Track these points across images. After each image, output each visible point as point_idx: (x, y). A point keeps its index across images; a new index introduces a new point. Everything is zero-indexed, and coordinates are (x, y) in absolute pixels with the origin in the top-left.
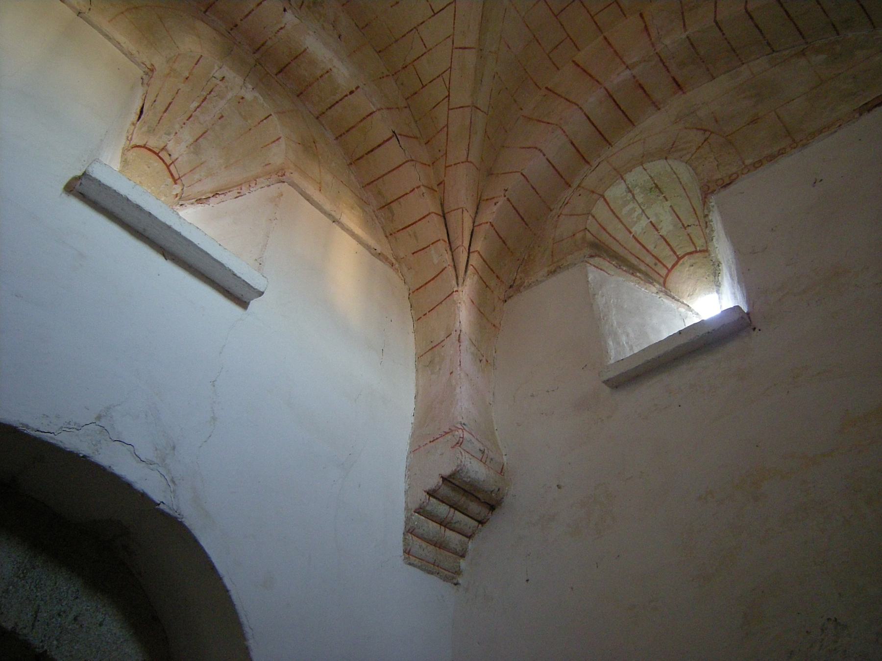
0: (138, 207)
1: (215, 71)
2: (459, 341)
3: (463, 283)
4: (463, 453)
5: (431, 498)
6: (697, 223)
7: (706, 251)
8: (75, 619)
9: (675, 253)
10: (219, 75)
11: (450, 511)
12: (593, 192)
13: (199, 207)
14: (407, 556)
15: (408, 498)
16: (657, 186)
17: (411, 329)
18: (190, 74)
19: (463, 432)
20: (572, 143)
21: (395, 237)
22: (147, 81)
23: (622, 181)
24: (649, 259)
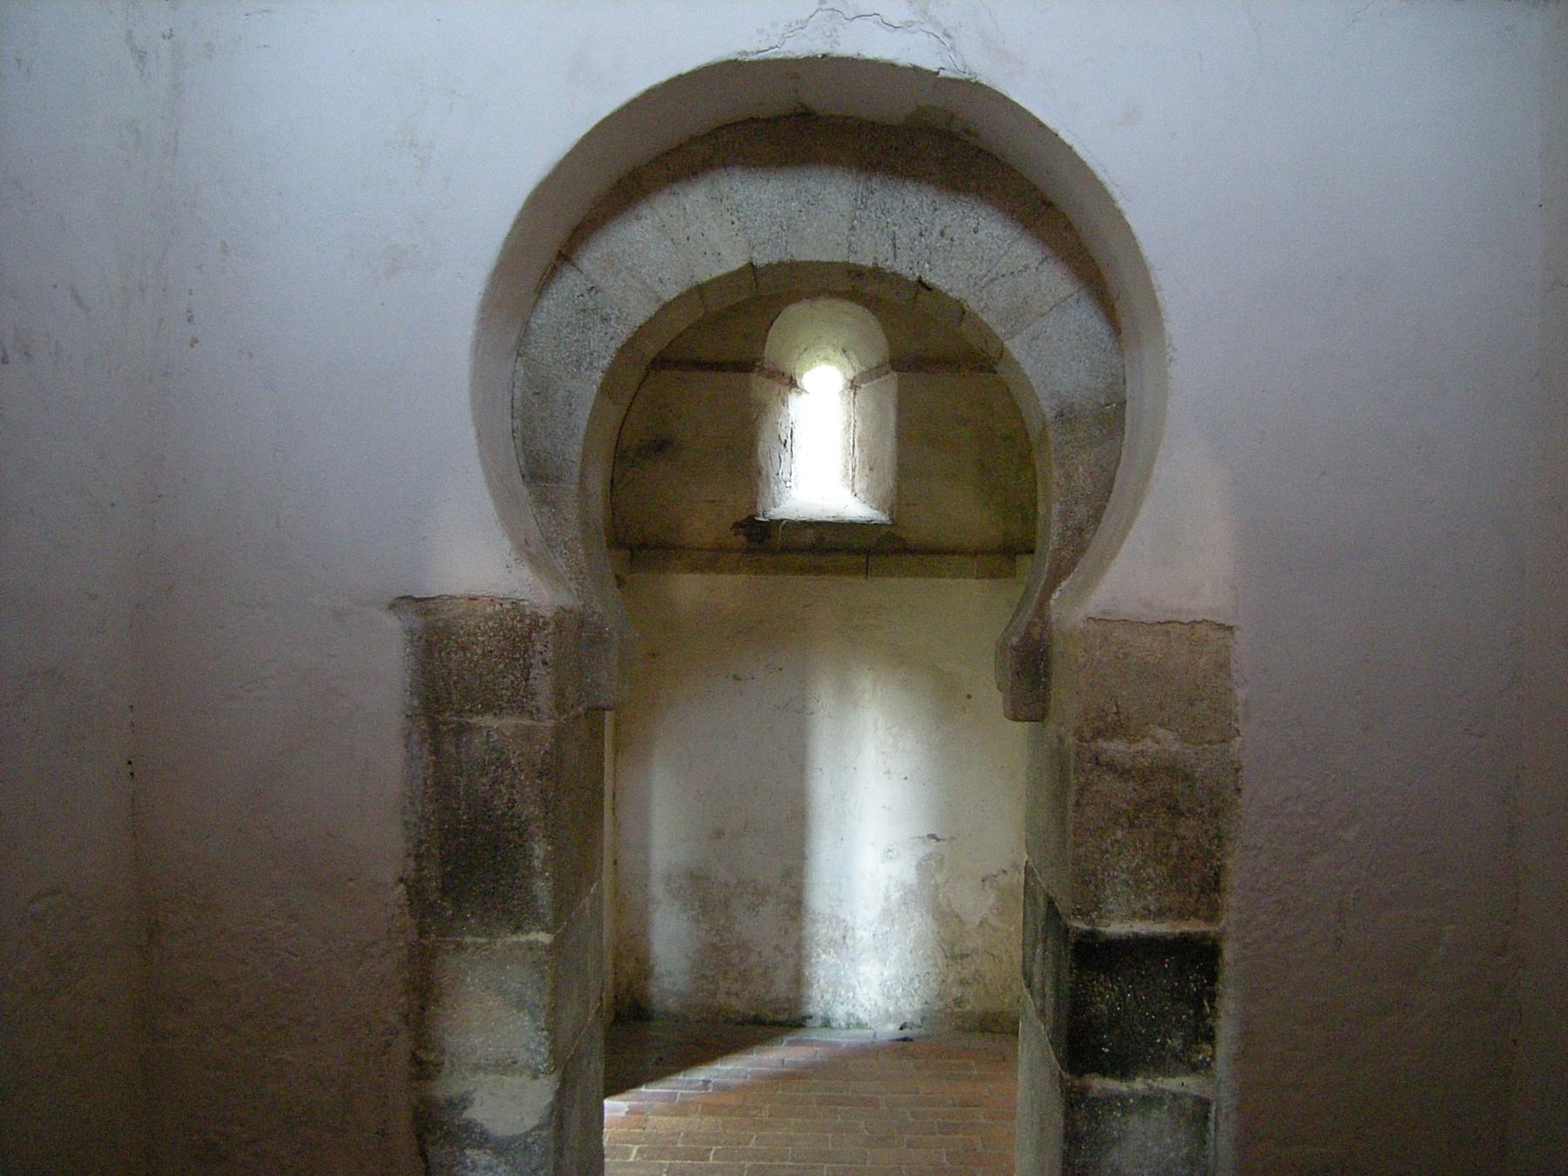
8: (942, 234)
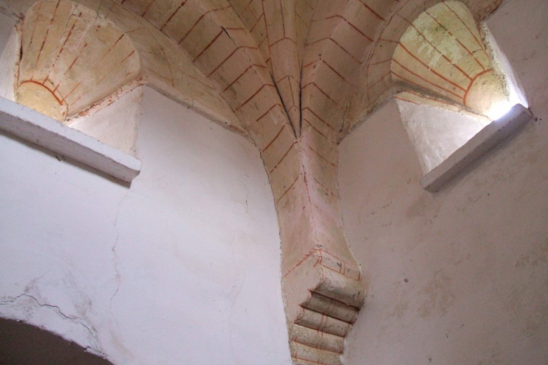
0: (29, 124)
1: (72, 10)
2: (305, 181)
3: (300, 135)
4: (323, 268)
5: (305, 310)
6: (480, 48)
7: (491, 70)
9: (468, 76)
10: (76, 12)
11: (323, 317)
12: (391, 41)
13: (82, 119)
14: (294, 359)
15: (288, 314)
16: (441, 26)
17: (267, 181)
18: (54, 16)
19: (321, 252)
20: (366, 6)
21: (241, 111)
22: (20, 27)
23: (412, 27)
24: (447, 86)
